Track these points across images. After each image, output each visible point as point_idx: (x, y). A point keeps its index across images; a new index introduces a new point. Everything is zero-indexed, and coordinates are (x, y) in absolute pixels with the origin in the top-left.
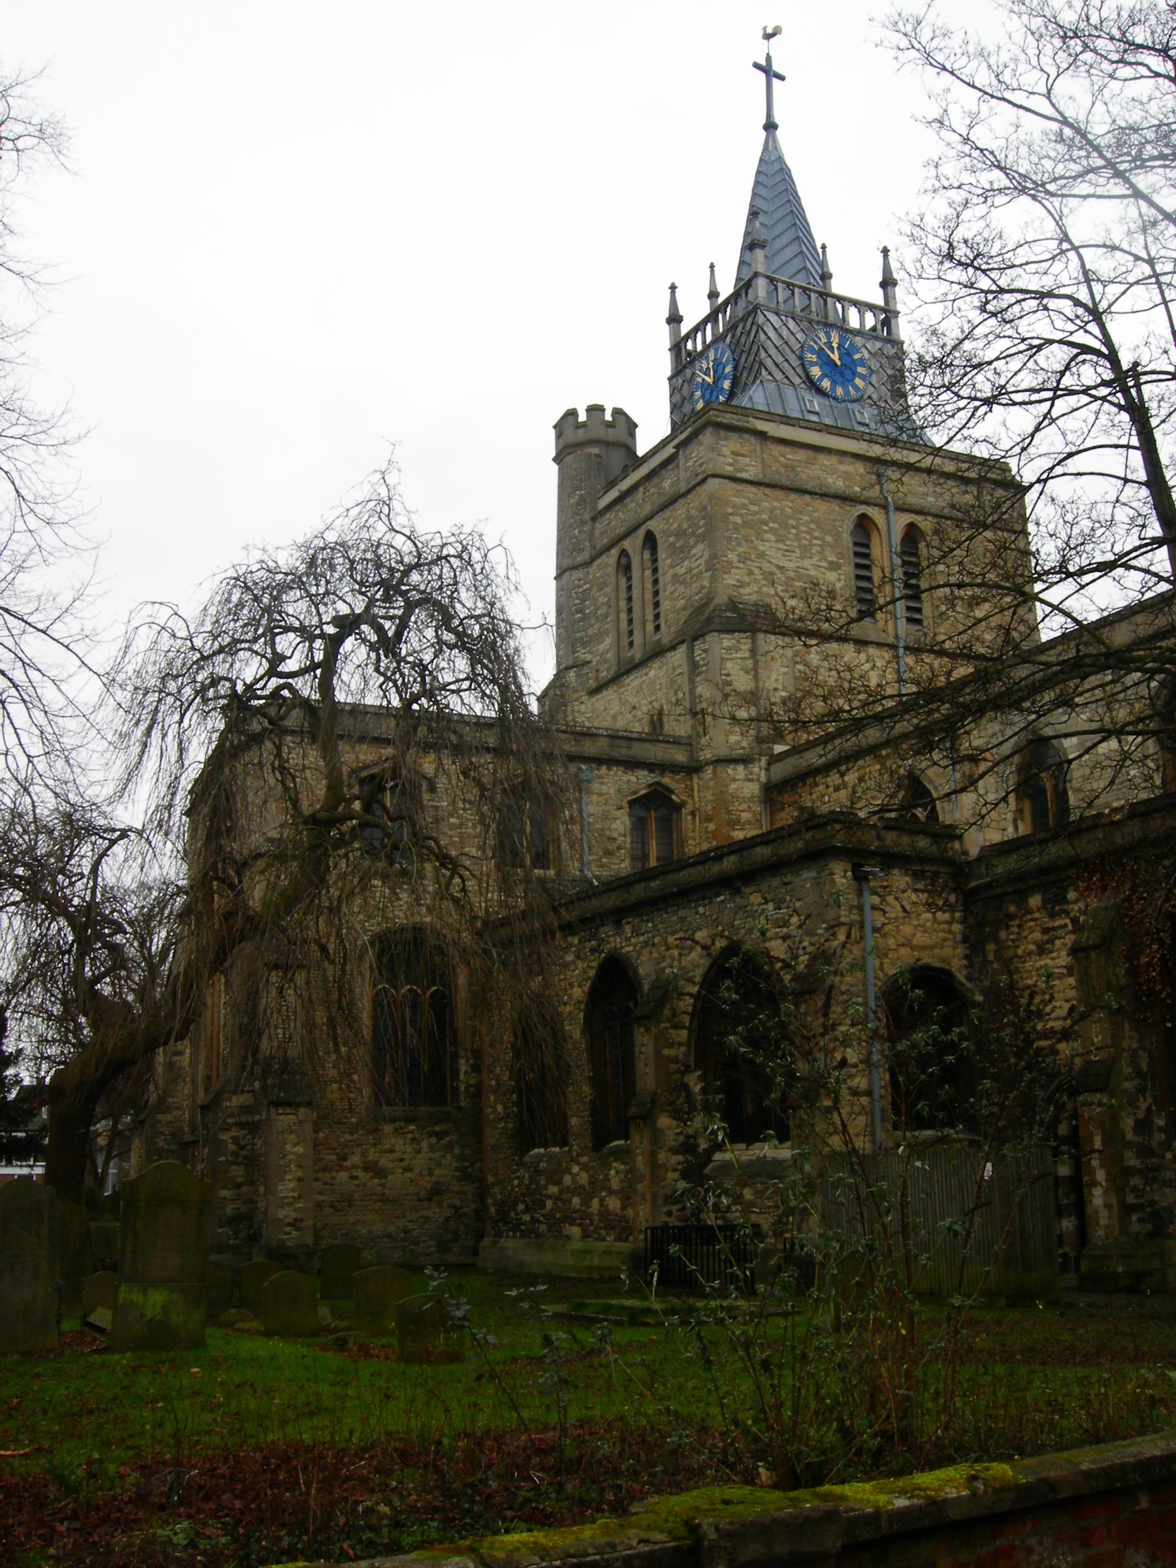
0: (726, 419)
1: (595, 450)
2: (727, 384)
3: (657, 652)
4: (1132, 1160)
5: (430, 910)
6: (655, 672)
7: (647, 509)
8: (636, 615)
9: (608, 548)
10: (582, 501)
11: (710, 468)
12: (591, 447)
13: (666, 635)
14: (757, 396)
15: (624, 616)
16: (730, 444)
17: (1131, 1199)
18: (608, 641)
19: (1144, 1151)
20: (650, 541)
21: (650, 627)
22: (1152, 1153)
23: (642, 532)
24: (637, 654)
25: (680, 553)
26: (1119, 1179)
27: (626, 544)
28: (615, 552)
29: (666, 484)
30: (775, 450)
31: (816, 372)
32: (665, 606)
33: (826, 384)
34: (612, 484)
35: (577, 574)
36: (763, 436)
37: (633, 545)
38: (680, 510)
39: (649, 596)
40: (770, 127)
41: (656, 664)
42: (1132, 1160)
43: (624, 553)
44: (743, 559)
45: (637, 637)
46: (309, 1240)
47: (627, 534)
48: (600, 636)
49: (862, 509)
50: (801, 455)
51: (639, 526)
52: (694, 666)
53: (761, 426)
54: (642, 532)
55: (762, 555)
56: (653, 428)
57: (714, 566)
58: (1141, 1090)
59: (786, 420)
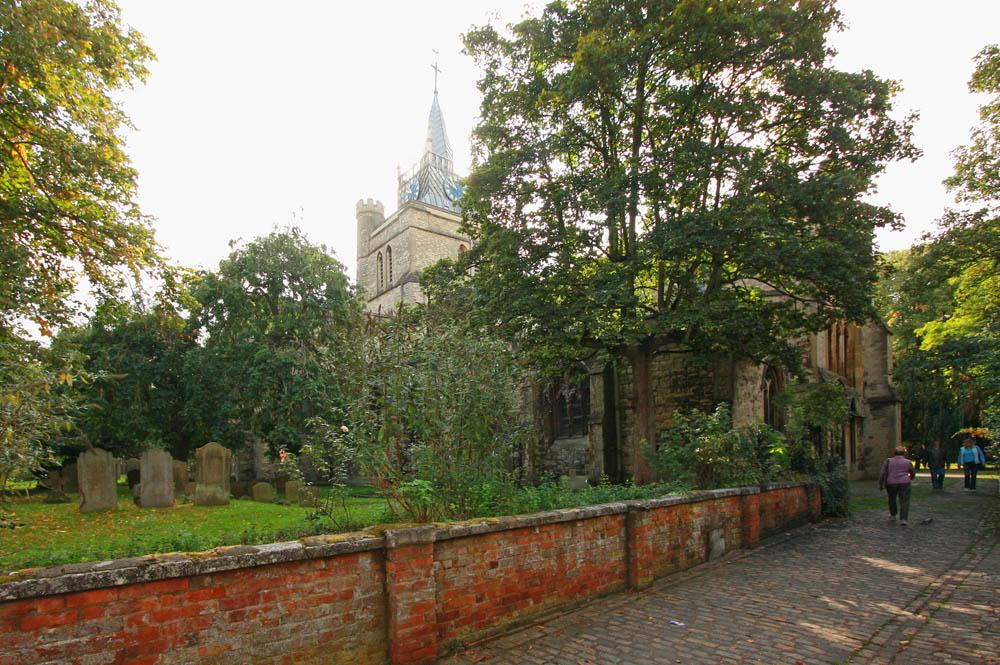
0: (416, 205)
1: (370, 215)
2: (417, 194)
3: (391, 288)
4: (537, 452)
5: (718, 348)
6: (391, 295)
7: (388, 238)
8: (384, 275)
9: (374, 251)
10: (365, 233)
11: (410, 224)
12: (370, 218)
13: (394, 283)
14: (427, 199)
15: (380, 275)
16: (418, 215)
17: (536, 464)
18: (375, 284)
19: (541, 449)
20: (389, 249)
21: (389, 280)
22: (544, 450)
23: (386, 246)
24: (384, 289)
25: (400, 254)
26: (533, 458)
27: (380, 250)
28: (377, 252)
29: (395, 229)
30: (431, 217)
31: (448, 191)
32: (394, 272)
33: (452, 196)
34: (376, 228)
35: (364, 260)
36: (429, 213)
37: (383, 250)
38: (400, 238)
39: (388, 268)
40: (436, 92)
41: (391, 292)
42: (537, 452)
43: (380, 253)
44: (421, 257)
45: (384, 283)
46: (274, 477)
47: (379, 247)
48: (372, 282)
49: (464, 243)
50: (442, 221)
51: (384, 244)
52: (403, 293)
53: (428, 209)
54: (386, 246)
55: (427, 257)
56: (390, 209)
57: (411, 259)
58: (542, 431)
59: (437, 208)
